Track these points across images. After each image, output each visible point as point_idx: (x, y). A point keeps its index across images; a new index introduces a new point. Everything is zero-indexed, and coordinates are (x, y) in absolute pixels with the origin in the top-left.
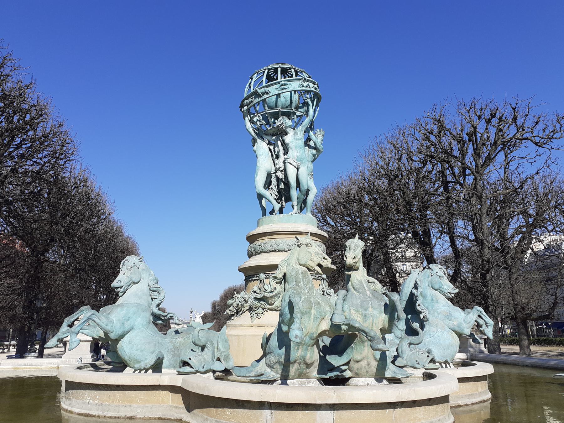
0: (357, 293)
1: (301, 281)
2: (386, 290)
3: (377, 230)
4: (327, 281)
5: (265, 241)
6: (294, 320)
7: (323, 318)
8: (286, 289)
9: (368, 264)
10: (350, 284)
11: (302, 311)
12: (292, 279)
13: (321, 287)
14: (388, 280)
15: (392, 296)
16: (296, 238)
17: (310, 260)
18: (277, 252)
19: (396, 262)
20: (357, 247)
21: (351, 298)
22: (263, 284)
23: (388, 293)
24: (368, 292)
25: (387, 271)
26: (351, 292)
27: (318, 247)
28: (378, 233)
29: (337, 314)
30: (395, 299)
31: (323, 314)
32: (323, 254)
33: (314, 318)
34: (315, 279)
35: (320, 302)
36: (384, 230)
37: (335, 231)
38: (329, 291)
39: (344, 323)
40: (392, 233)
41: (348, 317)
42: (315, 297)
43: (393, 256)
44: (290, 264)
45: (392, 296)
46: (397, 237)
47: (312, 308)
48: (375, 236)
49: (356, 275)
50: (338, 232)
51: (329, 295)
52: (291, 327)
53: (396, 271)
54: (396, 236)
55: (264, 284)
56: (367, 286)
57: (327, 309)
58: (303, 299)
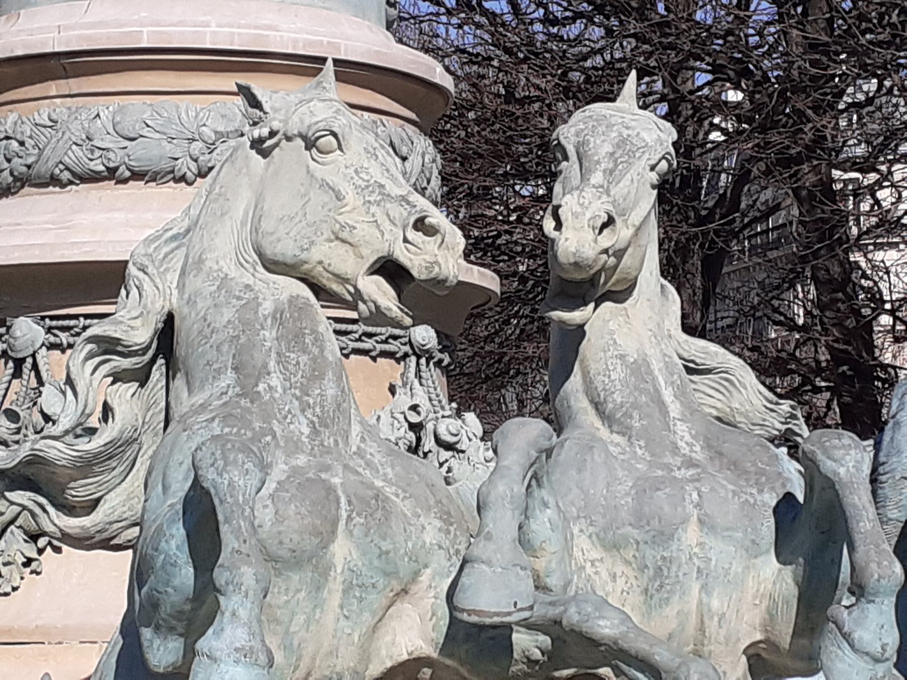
0: (617, 438)
1: (272, 364)
2: (793, 417)
3: (773, 48)
4: (439, 364)
5: (43, 112)
6: (222, 599)
7: (405, 591)
8: (176, 414)
9: (705, 260)
10: (575, 382)
11: (274, 548)
12: (212, 355)
13: (403, 400)
14: (824, 356)
15: (825, 451)
16: (245, 92)
17: (328, 234)
18: (125, 181)
19: (879, 247)
20: (631, 154)
21: (580, 471)
22: (34, 383)
23: (806, 432)
24: (681, 428)
25: (819, 304)
26: (576, 433)
27: (381, 153)
28: (778, 67)
29: (489, 563)
30: (842, 471)
31: (405, 567)
32: (416, 198)
33: (347, 590)
34: (365, 352)
35: (389, 491)
36: (813, 46)
37: (507, 51)
38: (454, 424)
39: (526, 614)
40: (863, 67)
41: (553, 581)
42: (357, 463)
43: (865, 207)
44: (200, 261)
45: (825, 451)
46: (890, 92)
47: (334, 532)
48: (757, 84)
49: (612, 325)
50: (526, 59)
51: (449, 447)
52: (202, 644)
53: (876, 299)
54: (888, 83)
55: (41, 383)
56: (681, 394)
57: (431, 536)
58: (279, 471)
